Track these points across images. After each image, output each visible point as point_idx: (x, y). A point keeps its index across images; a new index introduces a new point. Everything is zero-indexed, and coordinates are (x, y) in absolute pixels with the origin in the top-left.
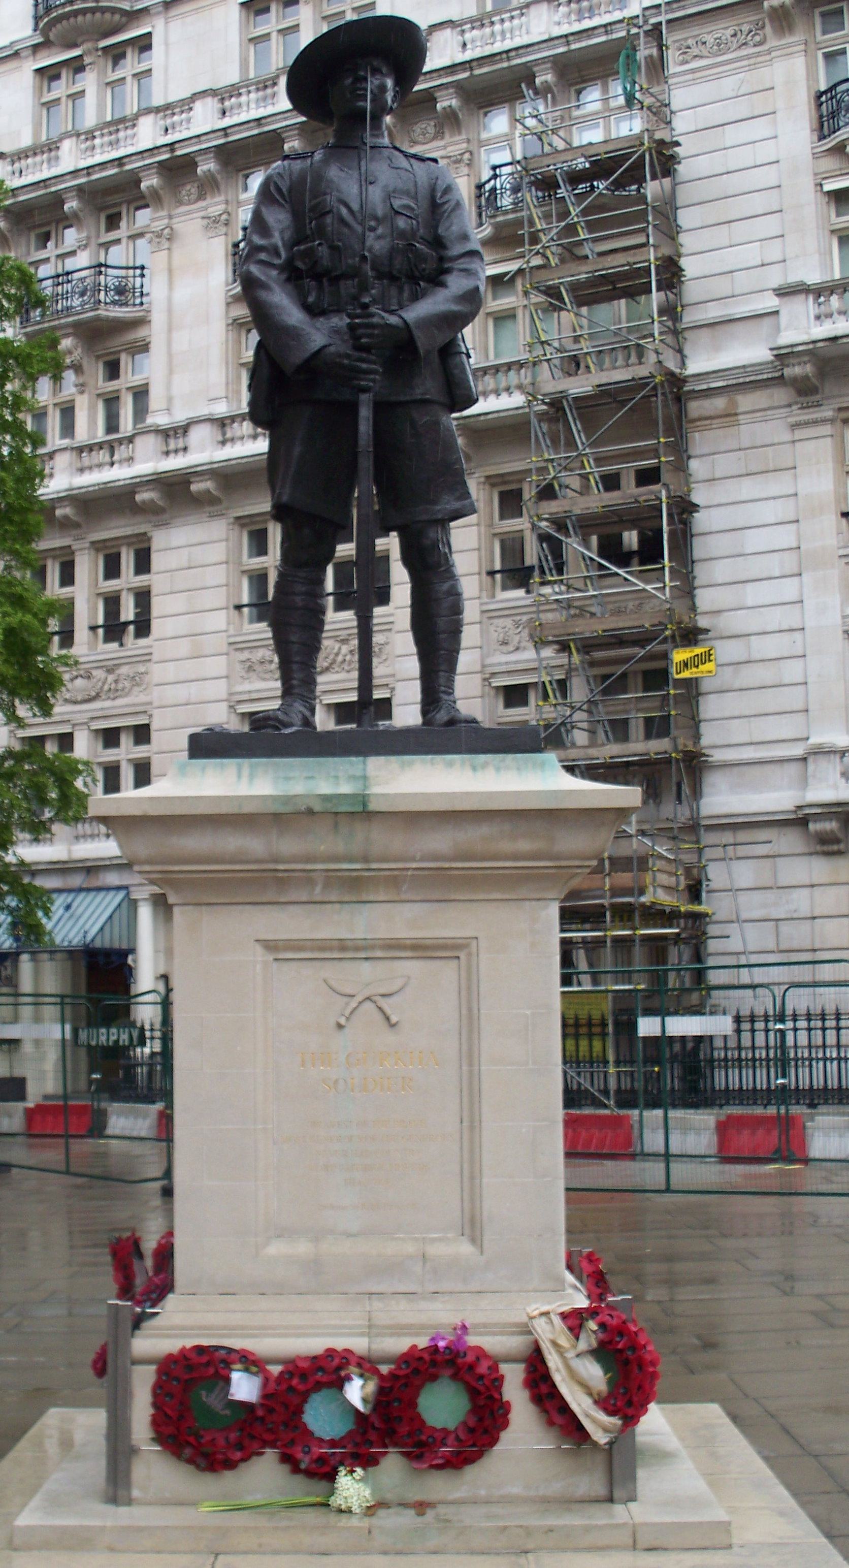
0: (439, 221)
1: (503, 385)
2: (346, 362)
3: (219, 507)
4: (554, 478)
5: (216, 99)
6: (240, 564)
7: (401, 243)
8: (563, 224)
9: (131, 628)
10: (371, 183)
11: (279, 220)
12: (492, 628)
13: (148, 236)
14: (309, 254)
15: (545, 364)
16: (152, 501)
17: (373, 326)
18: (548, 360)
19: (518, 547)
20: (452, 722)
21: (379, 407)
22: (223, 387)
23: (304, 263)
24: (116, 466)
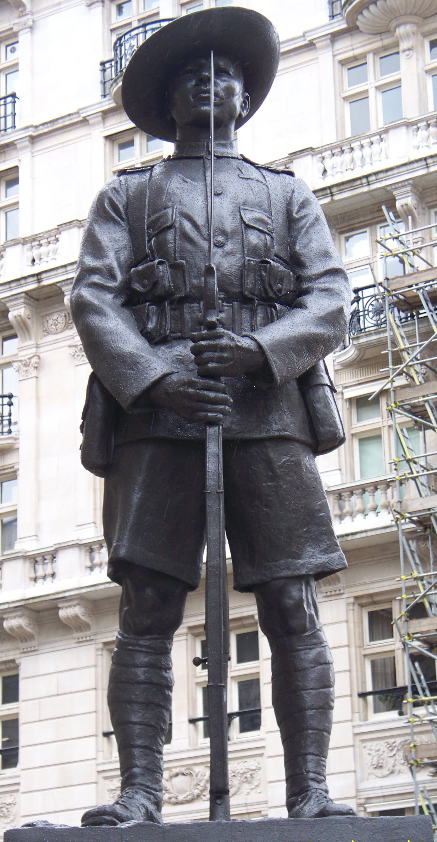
0: (296, 238)
1: (370, 504)
2: (191, 390)
3: (88, 633)
4: (425, 596)
7: (253, 261)
8: (426, 342)
10: (217, 195)
11: (114, 240)
12: (365, 752)
13: (15, 365)
14: (149, 274)
15: (412, 483)
16: (20, 627)
17: (223, 349)
18: (414, 479)
19: (389, 671)
20: (323, 813)
21: (228, 445)
22: (92, 512)
23: (144, 286)
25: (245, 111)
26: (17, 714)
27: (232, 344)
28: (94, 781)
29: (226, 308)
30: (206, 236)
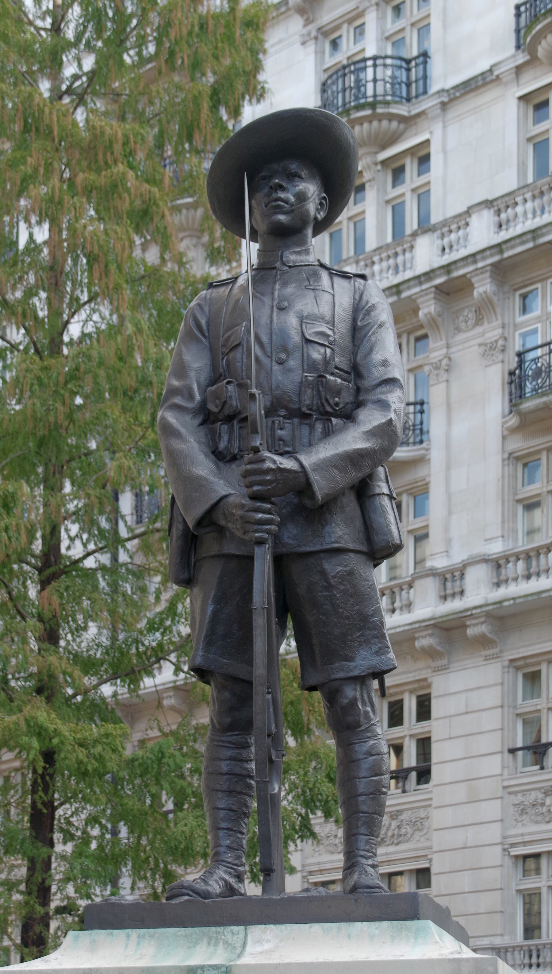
5: (492, 211)
6: (515, 707)
9: (414, 774)
21: (280, 562)
24: (397, 612)
25: (322, 213)
26: (430, 732)
27: (273, 467)
28: (499, 795)
29: (286, 425)
30: (269, 354)
